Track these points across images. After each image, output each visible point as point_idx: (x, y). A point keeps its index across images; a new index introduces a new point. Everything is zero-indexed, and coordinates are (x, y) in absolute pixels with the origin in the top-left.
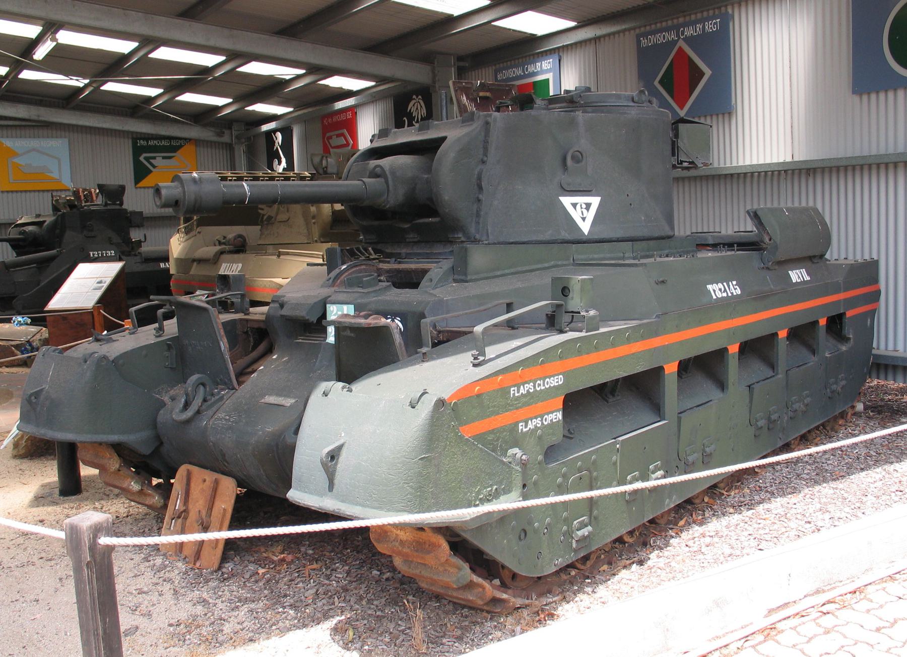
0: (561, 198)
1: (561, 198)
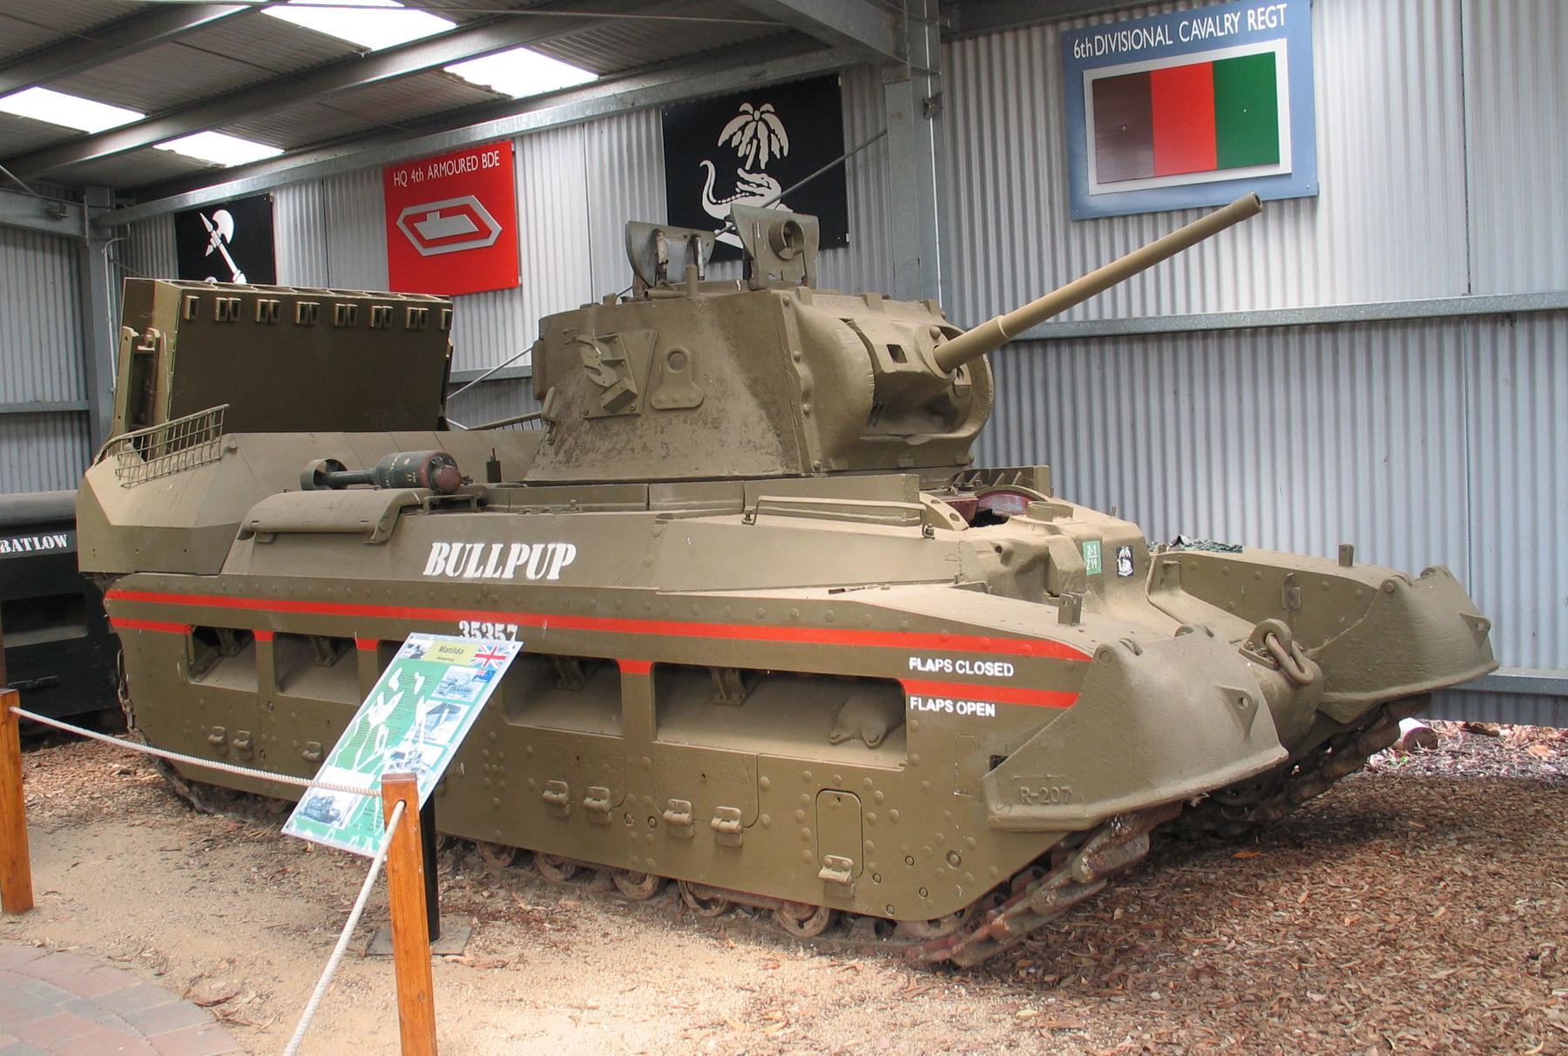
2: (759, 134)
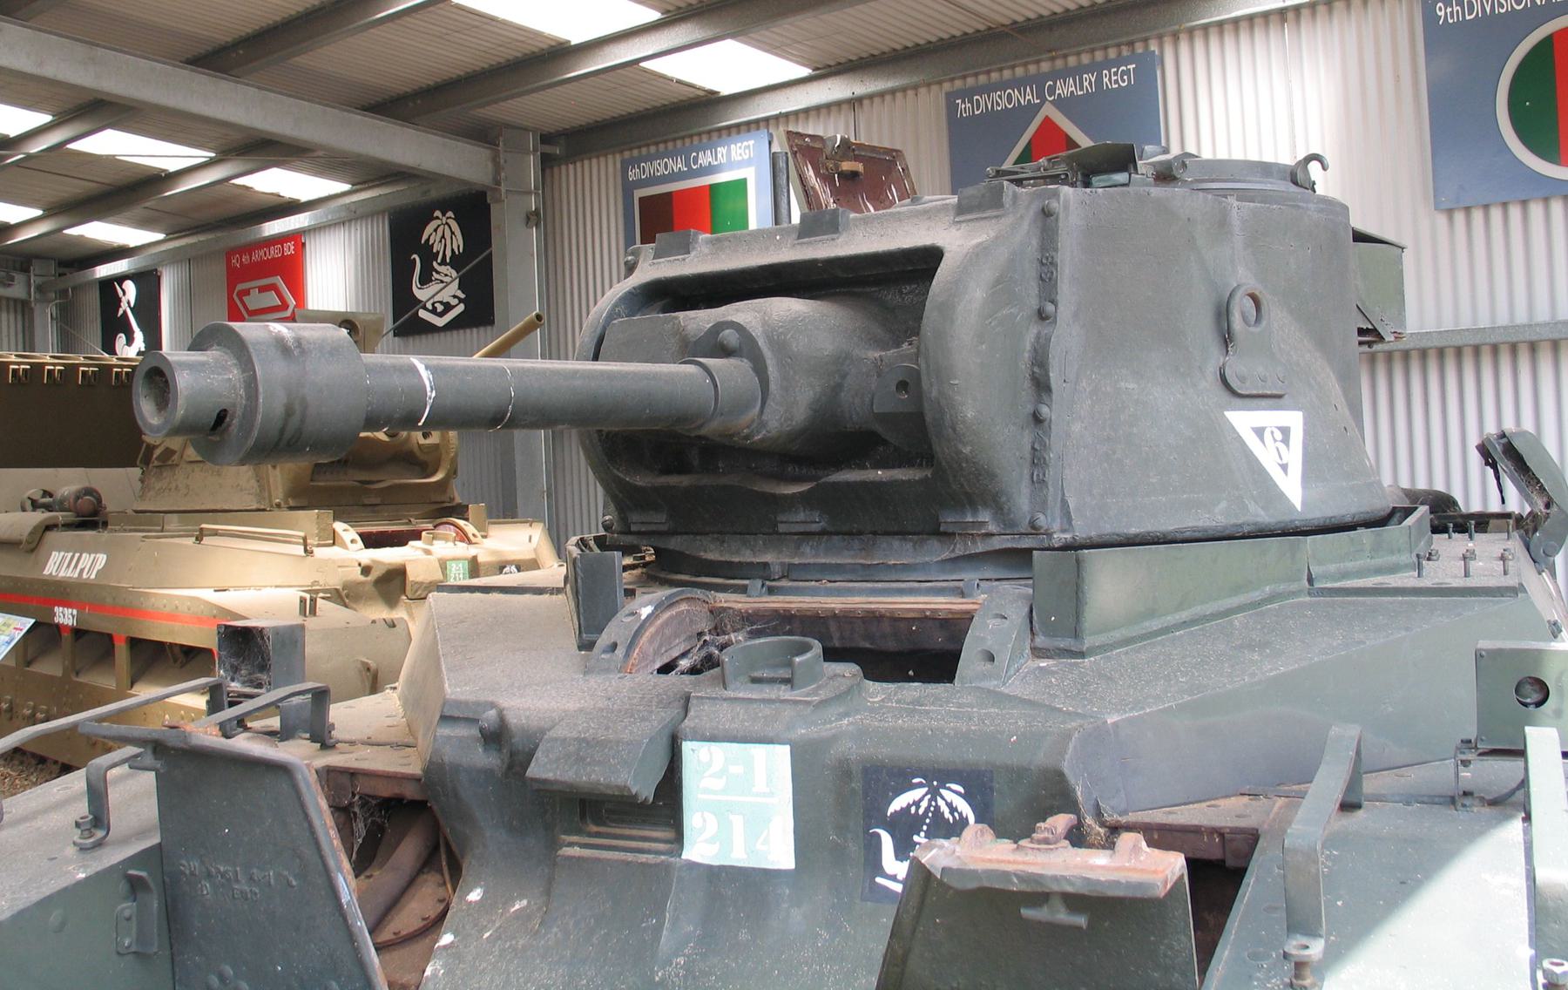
0: (1227, 414)
1: (1227, 414)
2: (445, 235)
